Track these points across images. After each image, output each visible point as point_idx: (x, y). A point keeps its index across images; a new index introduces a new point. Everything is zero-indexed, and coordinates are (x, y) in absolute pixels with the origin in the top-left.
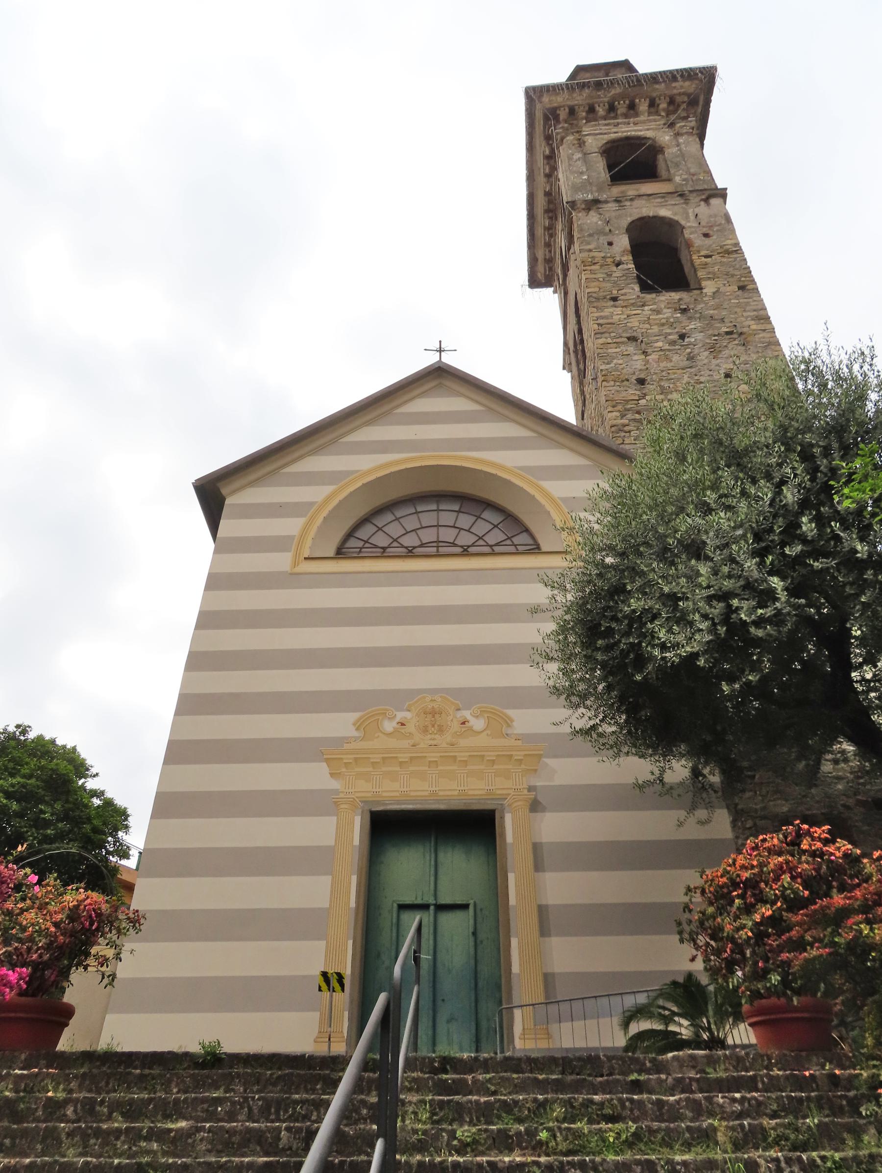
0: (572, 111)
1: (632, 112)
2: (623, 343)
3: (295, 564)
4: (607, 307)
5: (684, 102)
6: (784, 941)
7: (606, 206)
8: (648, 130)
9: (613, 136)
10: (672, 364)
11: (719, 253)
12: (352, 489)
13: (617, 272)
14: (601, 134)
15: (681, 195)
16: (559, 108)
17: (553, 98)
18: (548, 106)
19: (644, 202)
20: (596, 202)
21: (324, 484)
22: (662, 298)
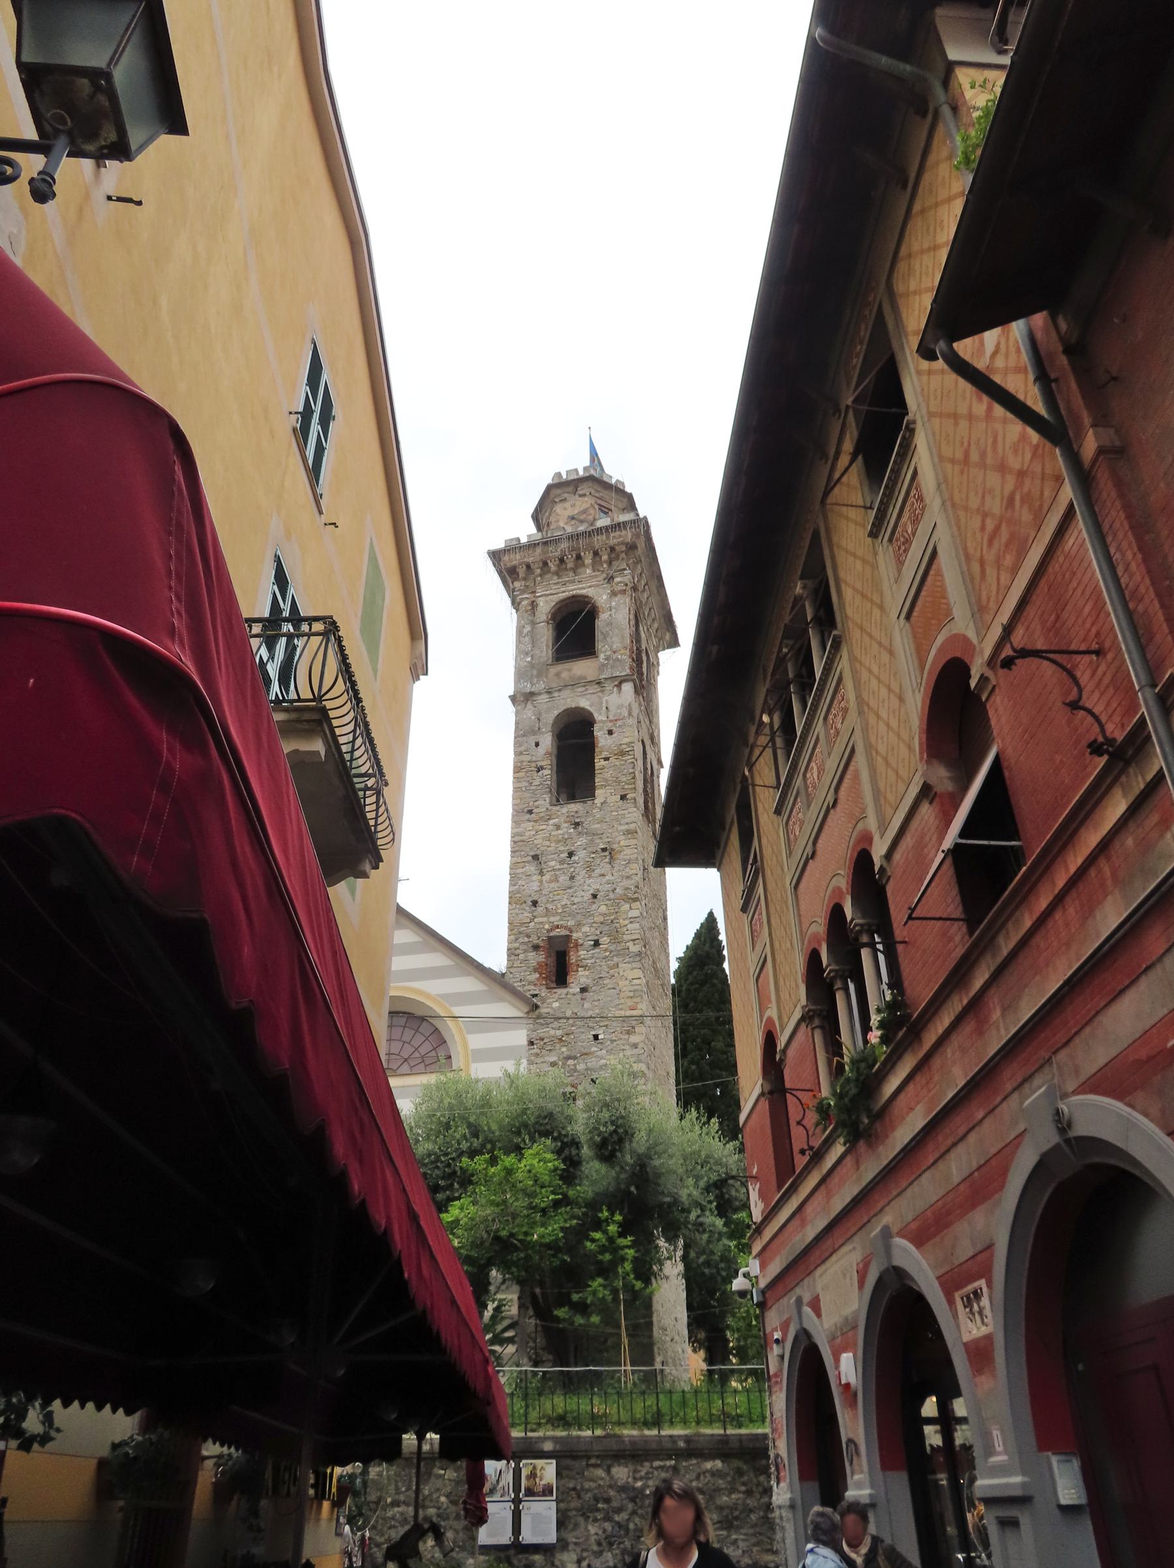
2: (528, 862)
6: (229, 1448)
7: (539, 698)
8: (590, 587)
10: (557, 884)
11: (615, 755)
14: (551, 594)
15: (598, 683)
18: (509, 565)
20: (532, 694)
22: (564, 810)
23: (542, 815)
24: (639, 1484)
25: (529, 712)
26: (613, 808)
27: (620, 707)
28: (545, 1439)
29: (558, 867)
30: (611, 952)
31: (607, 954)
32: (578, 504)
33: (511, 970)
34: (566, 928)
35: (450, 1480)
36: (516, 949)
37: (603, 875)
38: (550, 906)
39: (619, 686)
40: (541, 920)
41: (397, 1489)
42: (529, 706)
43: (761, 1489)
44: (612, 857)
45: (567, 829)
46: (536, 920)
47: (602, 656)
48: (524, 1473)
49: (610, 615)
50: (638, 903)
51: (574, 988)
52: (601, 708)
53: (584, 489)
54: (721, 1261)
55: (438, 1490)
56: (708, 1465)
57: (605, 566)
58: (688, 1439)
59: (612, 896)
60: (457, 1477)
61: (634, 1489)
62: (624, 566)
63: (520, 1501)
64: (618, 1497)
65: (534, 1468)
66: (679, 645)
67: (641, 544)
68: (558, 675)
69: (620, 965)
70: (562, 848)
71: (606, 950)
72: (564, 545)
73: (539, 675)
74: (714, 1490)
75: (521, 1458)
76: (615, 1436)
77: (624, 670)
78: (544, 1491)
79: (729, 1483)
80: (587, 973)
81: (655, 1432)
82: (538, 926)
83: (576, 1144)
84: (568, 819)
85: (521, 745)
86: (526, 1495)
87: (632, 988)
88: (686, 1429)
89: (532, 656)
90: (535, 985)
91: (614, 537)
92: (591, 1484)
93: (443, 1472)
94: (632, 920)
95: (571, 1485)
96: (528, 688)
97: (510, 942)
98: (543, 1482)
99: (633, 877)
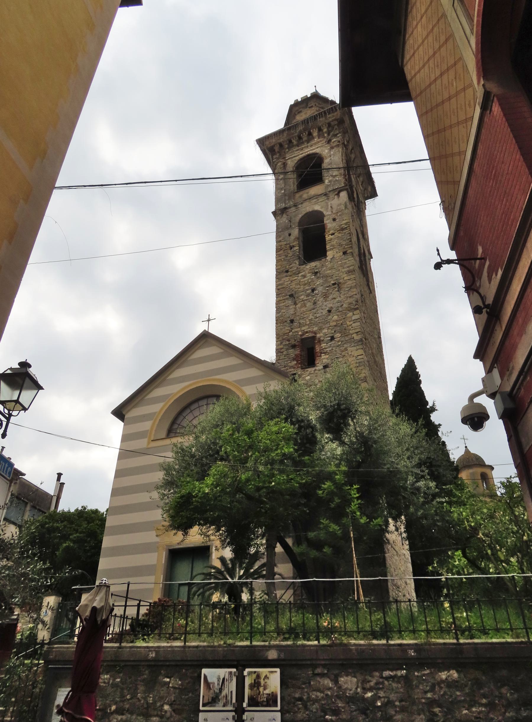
0: (281, 145)
1: (311, 137)
2: (287, 299)
3: (149, 443)
4: (283, 277)
5: (335, 125)
8: (317, 148)
9: (301, 156)
10: (306, 308)
12: (170, 403)
13: (290, 253)
16: (274, 146)
17: (271, 141)
18: (269, 146)
19: (307, 203)
20: (286, 208)
21: (159, 403)
22: (308, 267)
23: (294, 272)
24: (369, 695)
25: (284, 219)
26: (339, 260)
27: (340, 205)
28: (270, 647)
29: (306, 298)
30: (342, 342)
31: (340, 343)
32: (309, 111)
33: (279, 361)
34: (312, 332)
35: (174, 688)
36: (281, 349)
37: (335, 298)
38: (301, 321)
39: (338, 195)
40: (296, 330)
41: (123, 696)
42: (284, 215)
43: (504, 702)
44: (339, 287)
45: (310, 277)
46: (293, 331)
47: (327, 181)
48: (248, 682)
49: (331, 159)
50: (358, 311)
51: (320, 367)
52: (327, 209)
53: (312, 103)
54: (437, 514)
55: (161, 698)
56: (443, 675)
57: (326, 135)
58: (417, 648)
59: (340, 309)
60: (181, 685)
61: (364, 699)
62: (337, 132)
63: (244, 711)
64: (347, 708)
65: (258, 676)
66: (377, 195)
67: (346, 119)
68: (301, 197)
69: (349, 349)
70: (307, 288)
71: (339, 341)
72: (301, 128)
73: (289, 199)
74: (452, 702)
75: (245, 667)
76: (341, 644)
77: (341, 184)
78: (268, 700)
79: (468, 694)
80: (327, 356)
81: (384, 642)
82: (294, 334)
83: (310, 426)
84: (311, 271)
85: (280, 237)
86: (249, 705)
87: (358, 361)
88: (415, 639)
89: (285, 190)
90: (294, 368)
91: (330, 117)
92: (318, 694)
93: (168, 680)
94: (355, 321)
95: (297, 695)
96: (283, 205)
97: (277, 345)
98: (267, 692)
99: (355, 296)
